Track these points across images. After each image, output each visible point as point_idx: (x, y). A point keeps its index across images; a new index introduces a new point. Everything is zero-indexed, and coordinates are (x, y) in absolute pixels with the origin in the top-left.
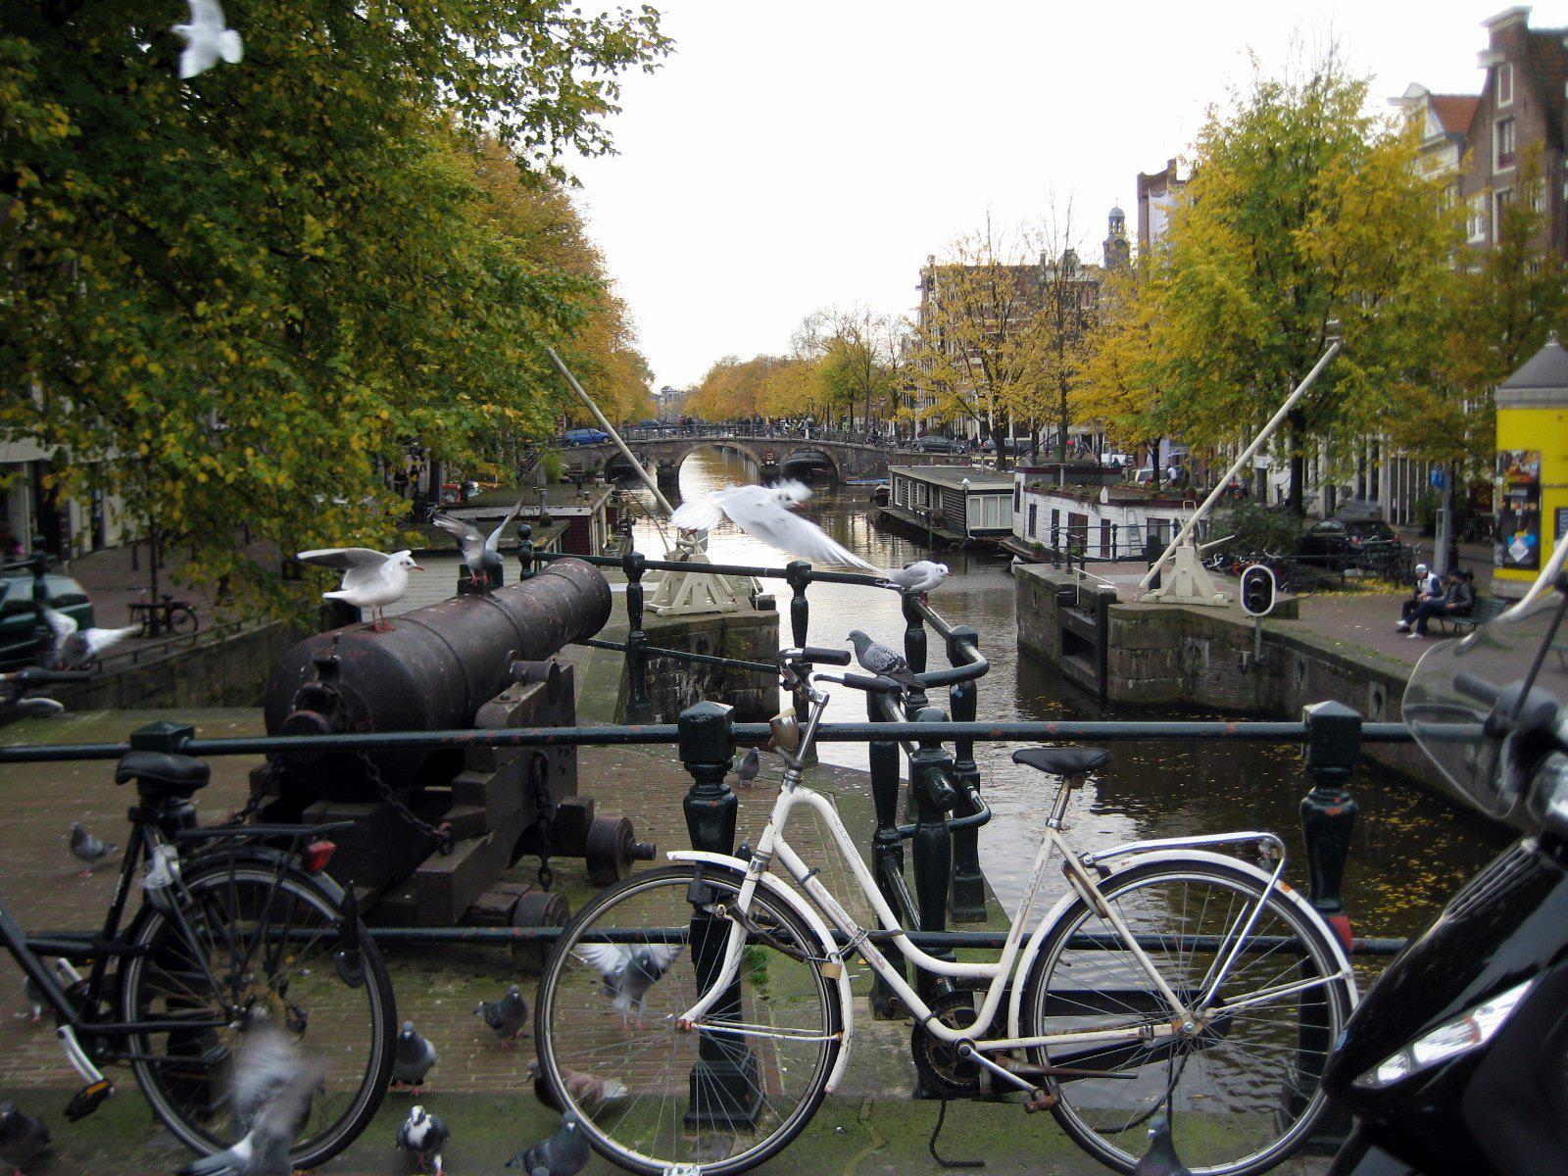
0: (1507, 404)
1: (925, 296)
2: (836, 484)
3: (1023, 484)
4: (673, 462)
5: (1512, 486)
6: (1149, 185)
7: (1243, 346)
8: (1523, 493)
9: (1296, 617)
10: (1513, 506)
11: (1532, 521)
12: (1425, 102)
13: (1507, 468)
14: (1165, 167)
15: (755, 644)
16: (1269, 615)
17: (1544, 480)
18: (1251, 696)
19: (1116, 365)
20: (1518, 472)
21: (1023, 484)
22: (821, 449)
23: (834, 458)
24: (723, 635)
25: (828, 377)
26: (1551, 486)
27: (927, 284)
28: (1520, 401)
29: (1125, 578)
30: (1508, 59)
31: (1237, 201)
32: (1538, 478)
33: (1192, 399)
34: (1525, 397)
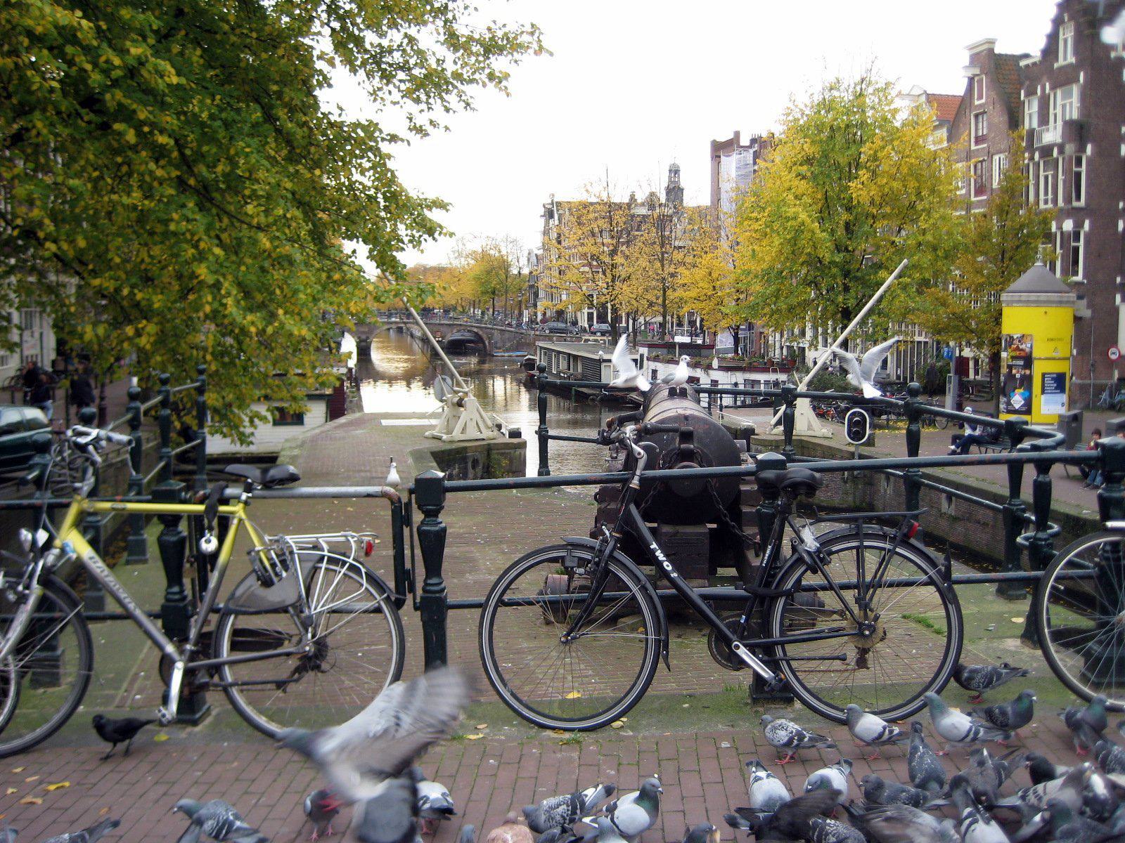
0: (1010, 303)
1: (547, 223)
2: (485, 356)
3: (646, 355)
4: (368, 338)
5: (1013, 358)
6: (720, 149)
7: (816, 262)
8: (1021, 363)
9: (874, 445)
10: (1014, 371)
11: (1027, 382)
12: (923, 98)
13: (1010, 346)
14: (731, 136)
15: (511, 461)
16: (862, 444)
17: (1034, 355)
18: (850, 499)
19: (710, 274)
20: (1018, 349)
21: (646, 355)
22: (475, 330)
23: (484, 336)
24: (489, 455)
25: (477, 279)
26: (1040, 359)
27: (549, 214)
28: (1020, 301)
29: (760, 419)
30: (982, 72)
31: (808, 161)
32: (1031, 353)
33: (777, 297)
34: (1023, 299)
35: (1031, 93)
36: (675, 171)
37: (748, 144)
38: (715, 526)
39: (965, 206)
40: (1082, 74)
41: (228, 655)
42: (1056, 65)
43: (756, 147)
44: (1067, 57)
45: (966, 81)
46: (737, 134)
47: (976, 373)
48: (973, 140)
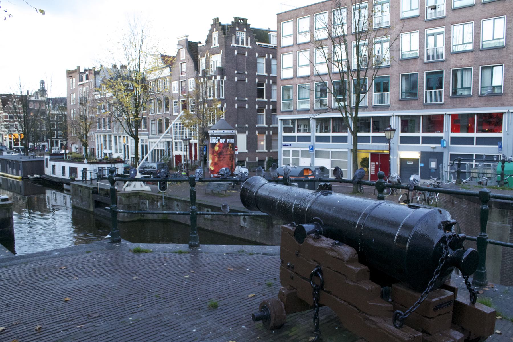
14: (76, 68)
35: (202, 56)
36: (43, 83)
37: (83, 71)
38: (257, 131)
39: (178, 98)
40: (221, 51)
41: (283, 109)
42: (212, 47)
43: (87, 73)
44: (215, 44)
45: (177, 50)
46: (79, 67)
47: (185, 161)
48: (180, 73)
